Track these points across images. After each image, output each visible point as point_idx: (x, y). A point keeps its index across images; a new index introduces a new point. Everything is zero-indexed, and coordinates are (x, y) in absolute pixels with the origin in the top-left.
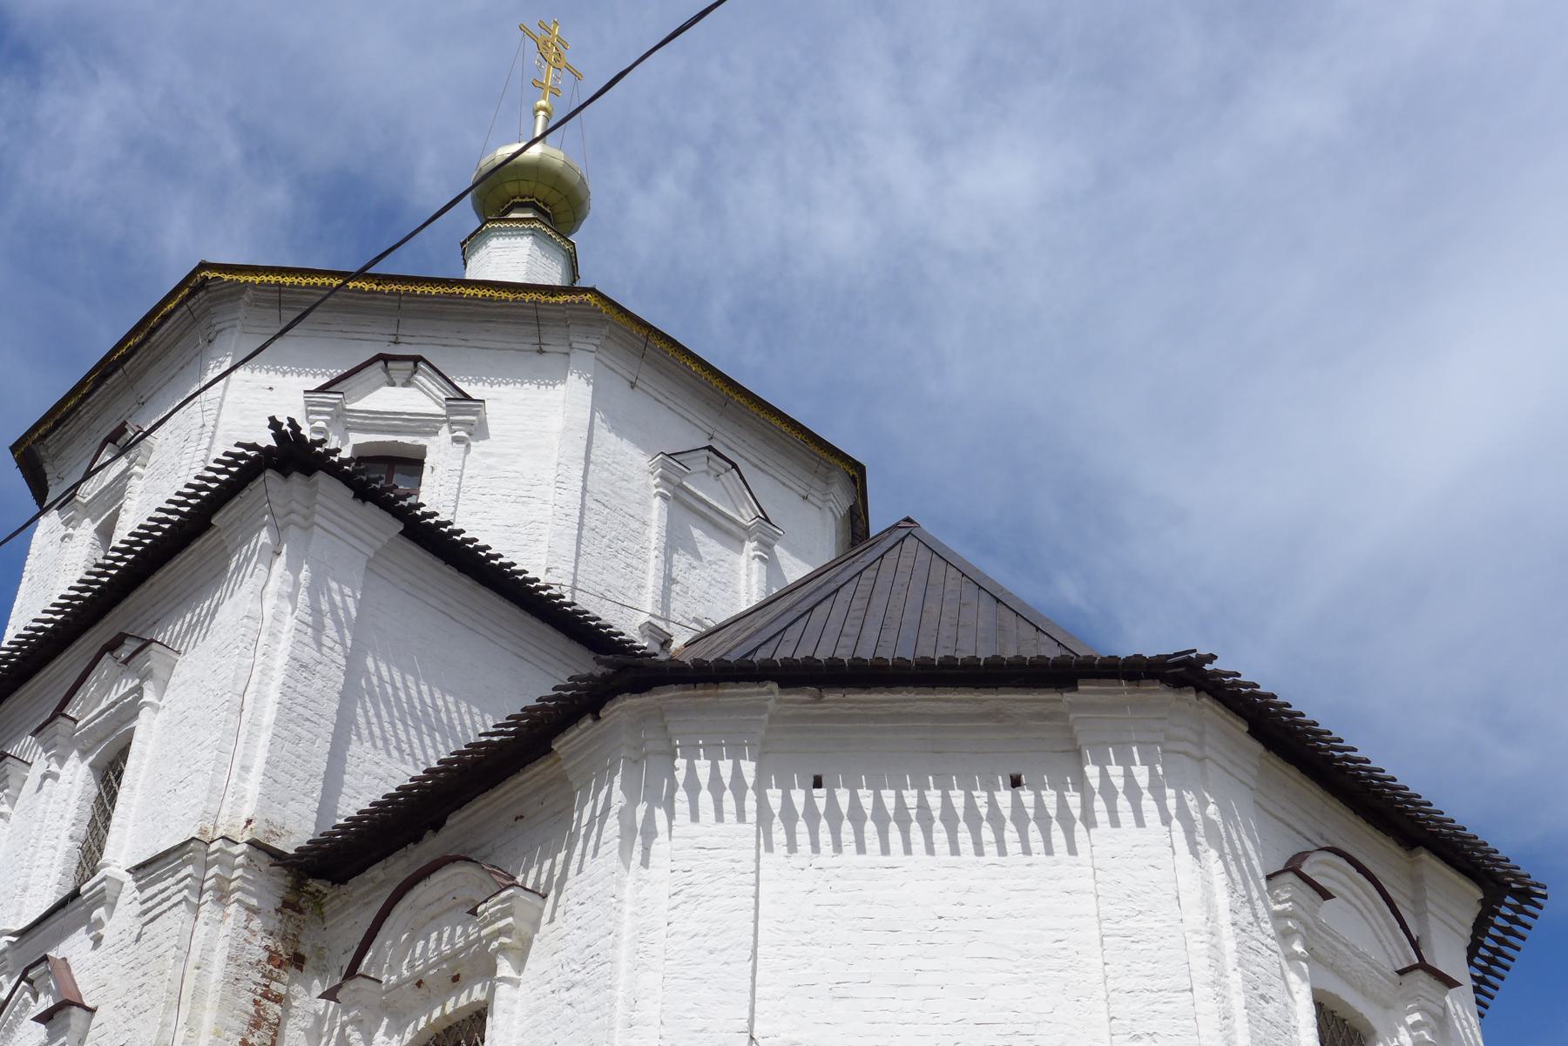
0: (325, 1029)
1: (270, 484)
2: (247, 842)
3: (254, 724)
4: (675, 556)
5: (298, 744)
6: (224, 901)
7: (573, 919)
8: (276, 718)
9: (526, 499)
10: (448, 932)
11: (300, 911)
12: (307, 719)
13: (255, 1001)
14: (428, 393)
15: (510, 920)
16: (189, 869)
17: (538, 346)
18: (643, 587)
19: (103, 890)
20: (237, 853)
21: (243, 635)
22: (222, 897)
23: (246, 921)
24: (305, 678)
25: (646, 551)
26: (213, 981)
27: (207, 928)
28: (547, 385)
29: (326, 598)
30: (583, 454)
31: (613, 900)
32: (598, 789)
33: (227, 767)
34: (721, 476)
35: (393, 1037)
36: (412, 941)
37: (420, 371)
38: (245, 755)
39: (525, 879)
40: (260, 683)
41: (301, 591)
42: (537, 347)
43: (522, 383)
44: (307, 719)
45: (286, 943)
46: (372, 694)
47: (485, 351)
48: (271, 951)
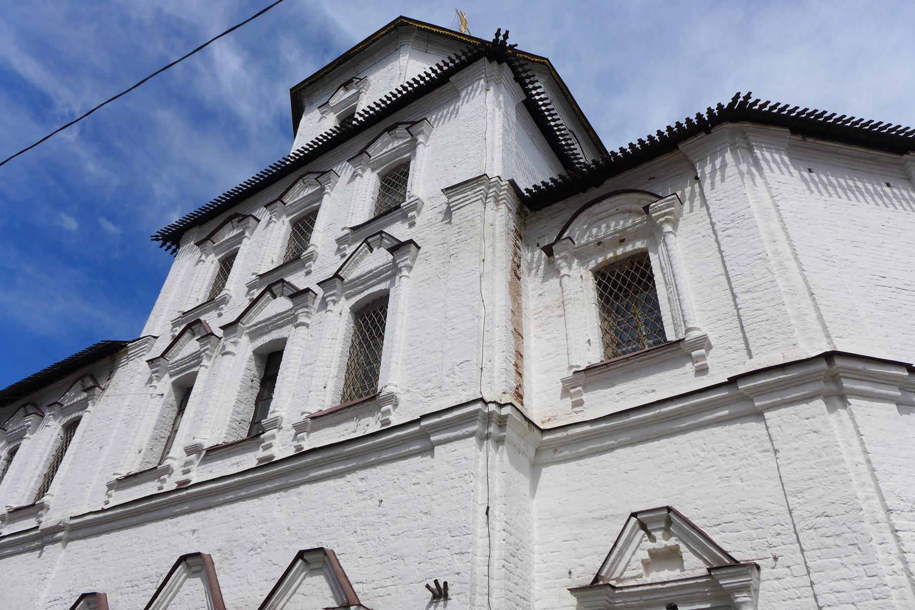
10: (614, 223)
15: (673, 208)
16: (483, 187)
19: (416, 204)
22: (497, 201)
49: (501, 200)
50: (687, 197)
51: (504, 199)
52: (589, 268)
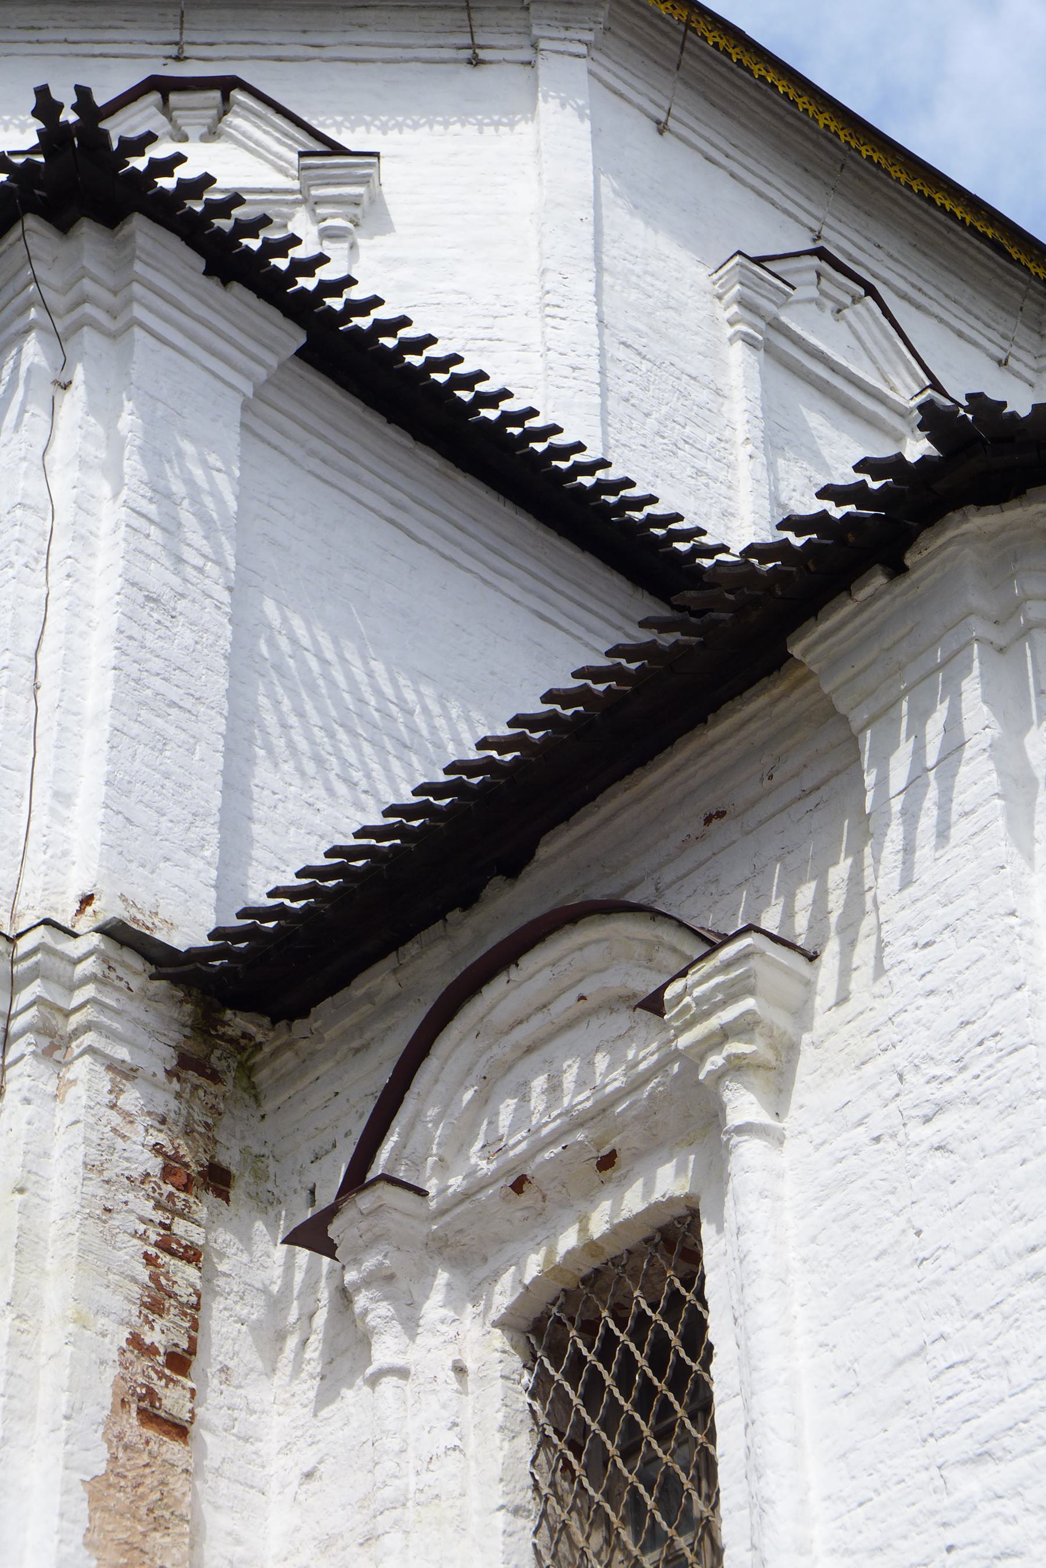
0: (293, 1317)
1: (32, 240)
2: (98, 930)
3: (68, 712)
4: (781, 462)
5: (161, 751)
6: (58, 1055)
7: (908, 978)
8: (114, 696)
9: (486, 343)
10: (575, 1070)
11: (215, 1077)
12: (173, 704)
13: (146, 1256)
14: (256, 151)
15: (749, 1003)
17: (471, 51)
18: (732, 515)
20: (76, 954)
21: (19, 541)
23: (111, 1092)
24: (159, 622)
25: (727, 446)
26: (54, 1216)
27: (29, 1111)
28: (497, 124)
29: (177, 471)
30: (589, 251)
31: (1012, 920)
32: (921, 715)
33: (22, 797)
34: (845, 312)
35: (463, 1307)
36: (484, 1100)
37: (235, 108)
38: (58, 771)
39: (789, 914)
40: (69, 631)
41: (126, 454)
42: (467, 54)
43: (446, 124)
44: (173, 704)
45: (194, 1140)
46: (279, 669)
47: (361, 66)
48: (165, 1155)
49: (76, 1033)
50: (295, 1293)
51: (88, 1027)
52: (494, 1315)
